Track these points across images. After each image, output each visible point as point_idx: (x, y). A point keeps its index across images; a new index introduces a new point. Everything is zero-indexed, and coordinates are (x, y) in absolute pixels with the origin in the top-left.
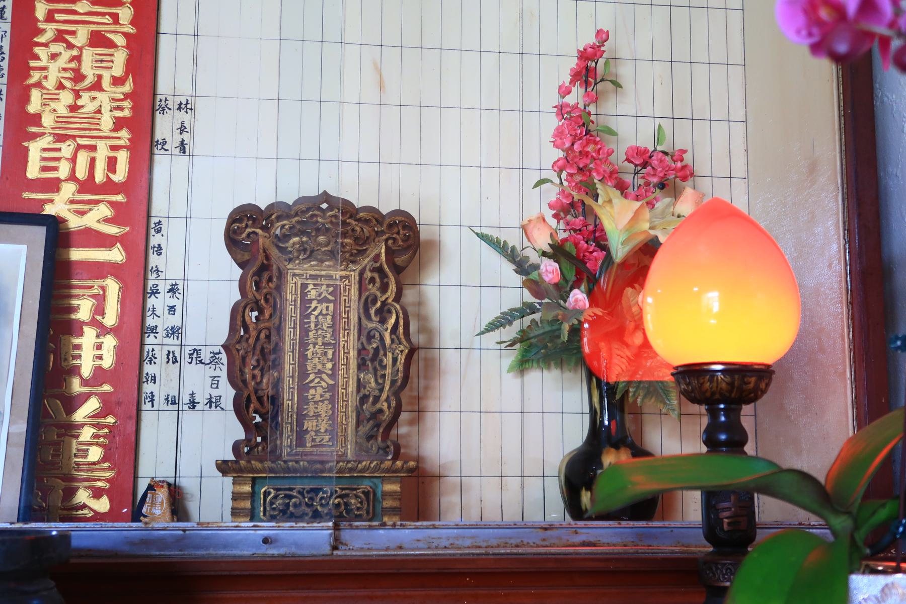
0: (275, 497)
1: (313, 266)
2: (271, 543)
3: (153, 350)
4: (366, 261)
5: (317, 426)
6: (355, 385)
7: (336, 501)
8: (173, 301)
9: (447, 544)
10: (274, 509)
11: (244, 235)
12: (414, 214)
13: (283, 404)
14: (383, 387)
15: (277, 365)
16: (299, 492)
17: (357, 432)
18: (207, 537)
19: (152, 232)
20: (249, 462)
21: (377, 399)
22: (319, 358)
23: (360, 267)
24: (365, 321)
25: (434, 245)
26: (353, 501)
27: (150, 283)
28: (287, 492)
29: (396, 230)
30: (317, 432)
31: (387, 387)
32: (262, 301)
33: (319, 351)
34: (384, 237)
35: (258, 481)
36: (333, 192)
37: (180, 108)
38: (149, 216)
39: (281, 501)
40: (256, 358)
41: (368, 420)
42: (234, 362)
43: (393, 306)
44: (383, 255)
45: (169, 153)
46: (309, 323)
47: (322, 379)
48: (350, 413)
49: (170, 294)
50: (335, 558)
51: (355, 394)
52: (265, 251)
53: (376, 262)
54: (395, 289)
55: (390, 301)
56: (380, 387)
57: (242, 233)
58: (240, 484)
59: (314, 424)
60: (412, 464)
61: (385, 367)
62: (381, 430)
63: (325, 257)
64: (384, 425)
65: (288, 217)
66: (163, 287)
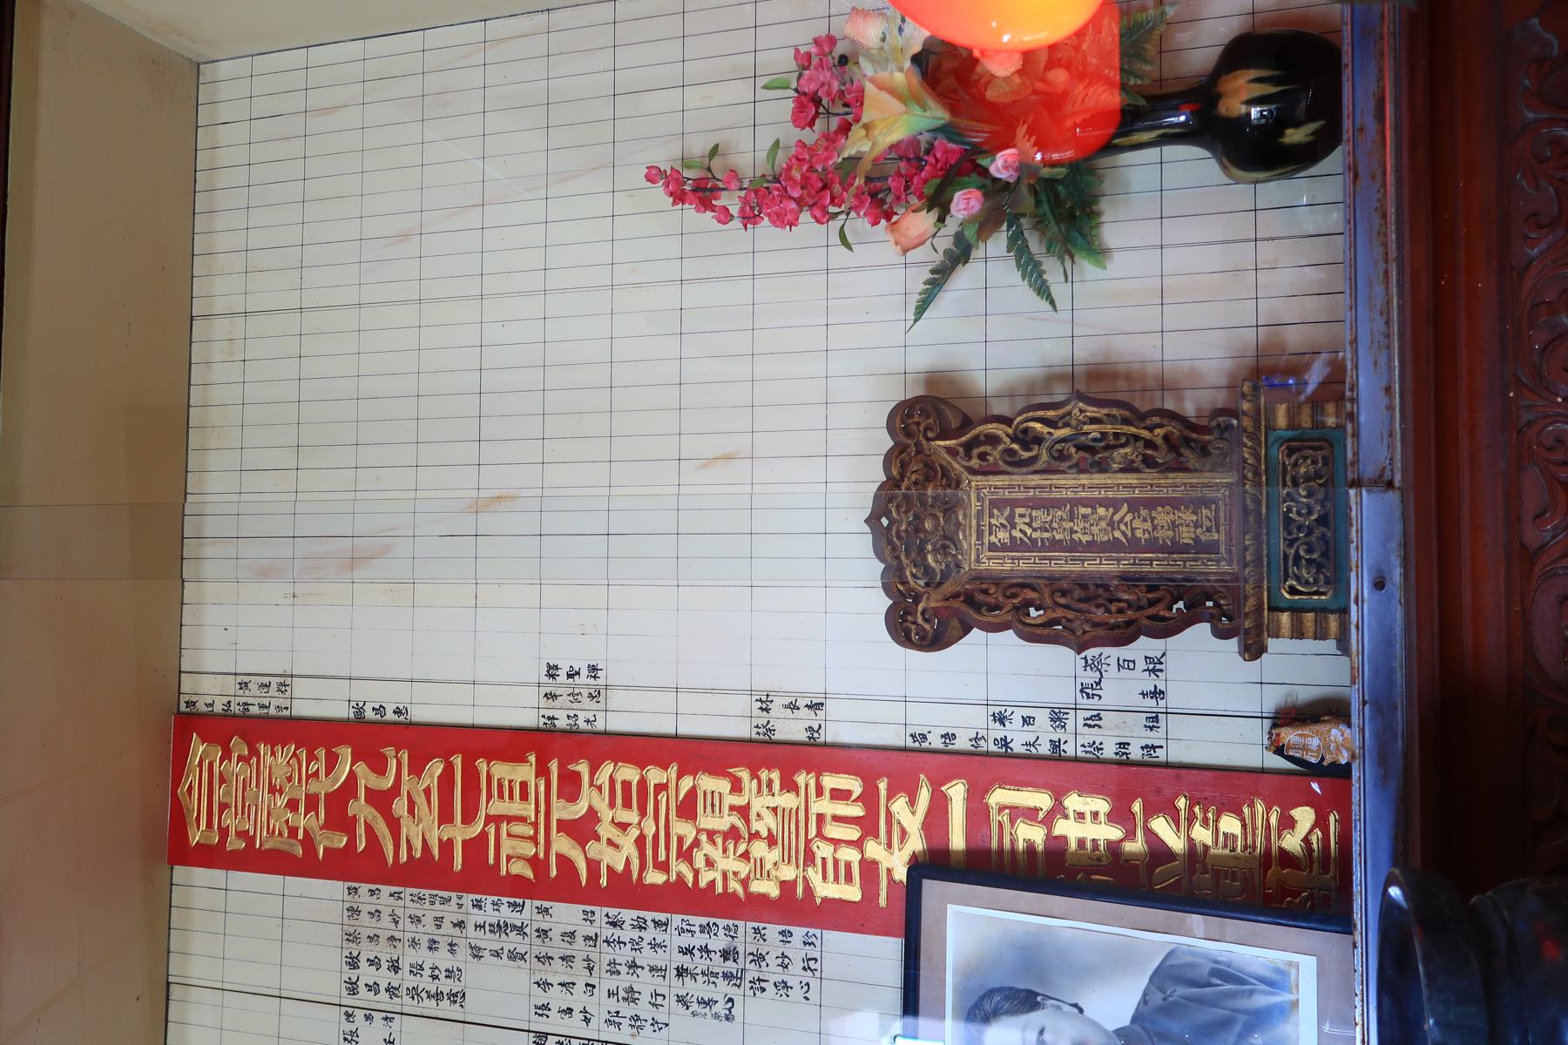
0: (1298, 579)
4: (957, 466)
10: (1316, 581)
11: (927, 626)
20: (1246, 615)
21: (1150, 444)
24: (1039, 465)
25: (934, 379)
26: (1303, 470)
27: (993, 748)
29: (914, 427)
30: (1197, 525)
31: (1133, 430)
35: (1273, 604)
37: (767, 710)
38: (905, 749)
55: (1010, 431)
58: (1279, 629)
62: (1195, 436)
64: (1187, 433)
65: (901, 569)
66: (998, 732)
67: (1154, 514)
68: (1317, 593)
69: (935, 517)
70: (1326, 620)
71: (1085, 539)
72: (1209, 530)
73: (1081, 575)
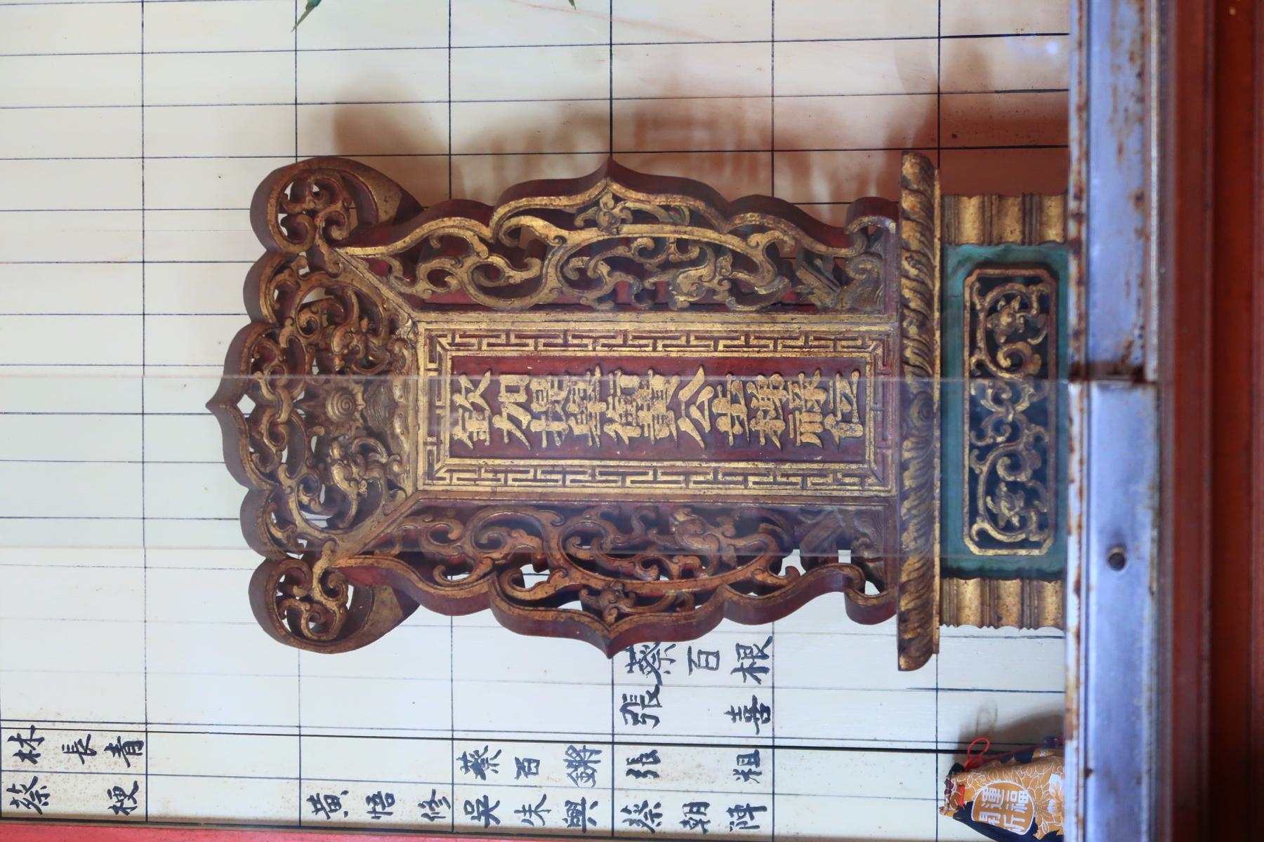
0: (993, 518)
1: (406, 428)
2: (1122, 545)
3: (626, 810)
4: (389, 294)
5: (810, 411)
6: (706, 316)
7: (1005, 363)
8: (507, 766)
9: (1130, 71)
10: (1024, 521)
11: (331, 604)
12: (265, 169)
13: (756, 498)
14: (708, 244)
15: (657, 518)
16: (981, 458)
17: (825, 310)
18: (1107, 715)
19: (337, 817)
20: (903, 588)
21: (741, 261)
22: (640, 408)
23: (405, 311)
24: (543, 296)
25: (350, 118)
26: (1005, 320)
27: (463, 819)
28: (981, 489)
29: (303, 220)
30: (826, 410)
31: (710, 235)
32: (496, 555)
33: (621, 408)
34: (324, 249)
35: (951, 563)
36: (211, 388)
37: (32, 757)
38: (300, 826)
39: (1004, 505)
40: (639, 570)
41: (795, 281)
42: (652, 626)
43: (499, 225)
44: (370, 251)
45: (141, 781)
46: (549, 434)
47: (691, 402)
48: (778, 328)
49: (488, 772)
50: (1170, 376)
51: (730, 317)
52: (371, 553)
53: (390, 269)
54: (457, 220)
55: (487, 232)
56: (710, 253)
57: (326, 610)
58: (959, 608)
59: (805, 417)
60: (909, 168)
61: (659, 242)
62: (821, 248)
63: (383, 398)
64: (808, 242)
65: (278, 500)
66: (471, 789)
67: (751, 389)
68: (1024, 544)
69: (347, 393)
70: (1040, 594)
71: (627, 433)
72: (847, 419)
73: (619, 503)
